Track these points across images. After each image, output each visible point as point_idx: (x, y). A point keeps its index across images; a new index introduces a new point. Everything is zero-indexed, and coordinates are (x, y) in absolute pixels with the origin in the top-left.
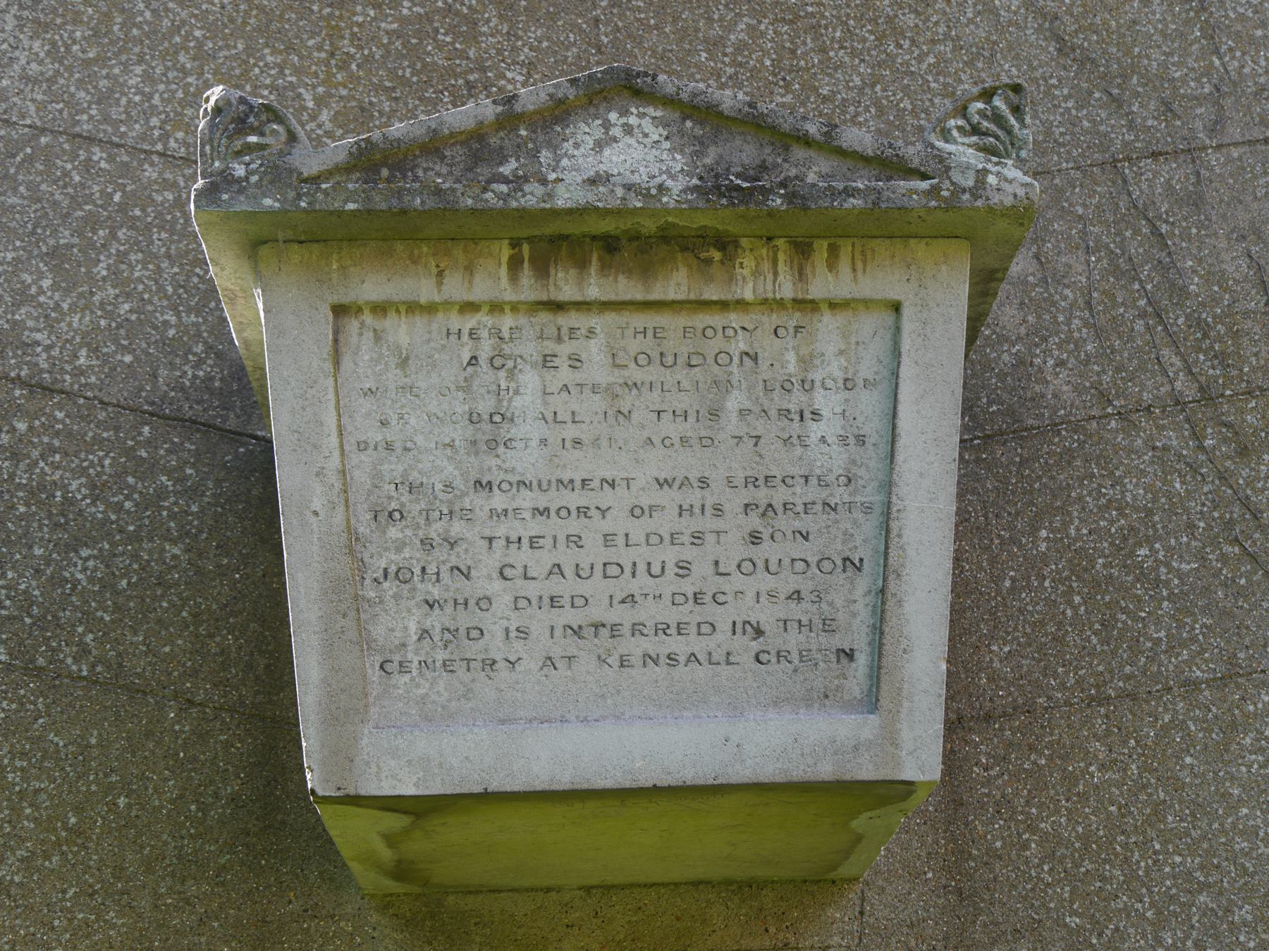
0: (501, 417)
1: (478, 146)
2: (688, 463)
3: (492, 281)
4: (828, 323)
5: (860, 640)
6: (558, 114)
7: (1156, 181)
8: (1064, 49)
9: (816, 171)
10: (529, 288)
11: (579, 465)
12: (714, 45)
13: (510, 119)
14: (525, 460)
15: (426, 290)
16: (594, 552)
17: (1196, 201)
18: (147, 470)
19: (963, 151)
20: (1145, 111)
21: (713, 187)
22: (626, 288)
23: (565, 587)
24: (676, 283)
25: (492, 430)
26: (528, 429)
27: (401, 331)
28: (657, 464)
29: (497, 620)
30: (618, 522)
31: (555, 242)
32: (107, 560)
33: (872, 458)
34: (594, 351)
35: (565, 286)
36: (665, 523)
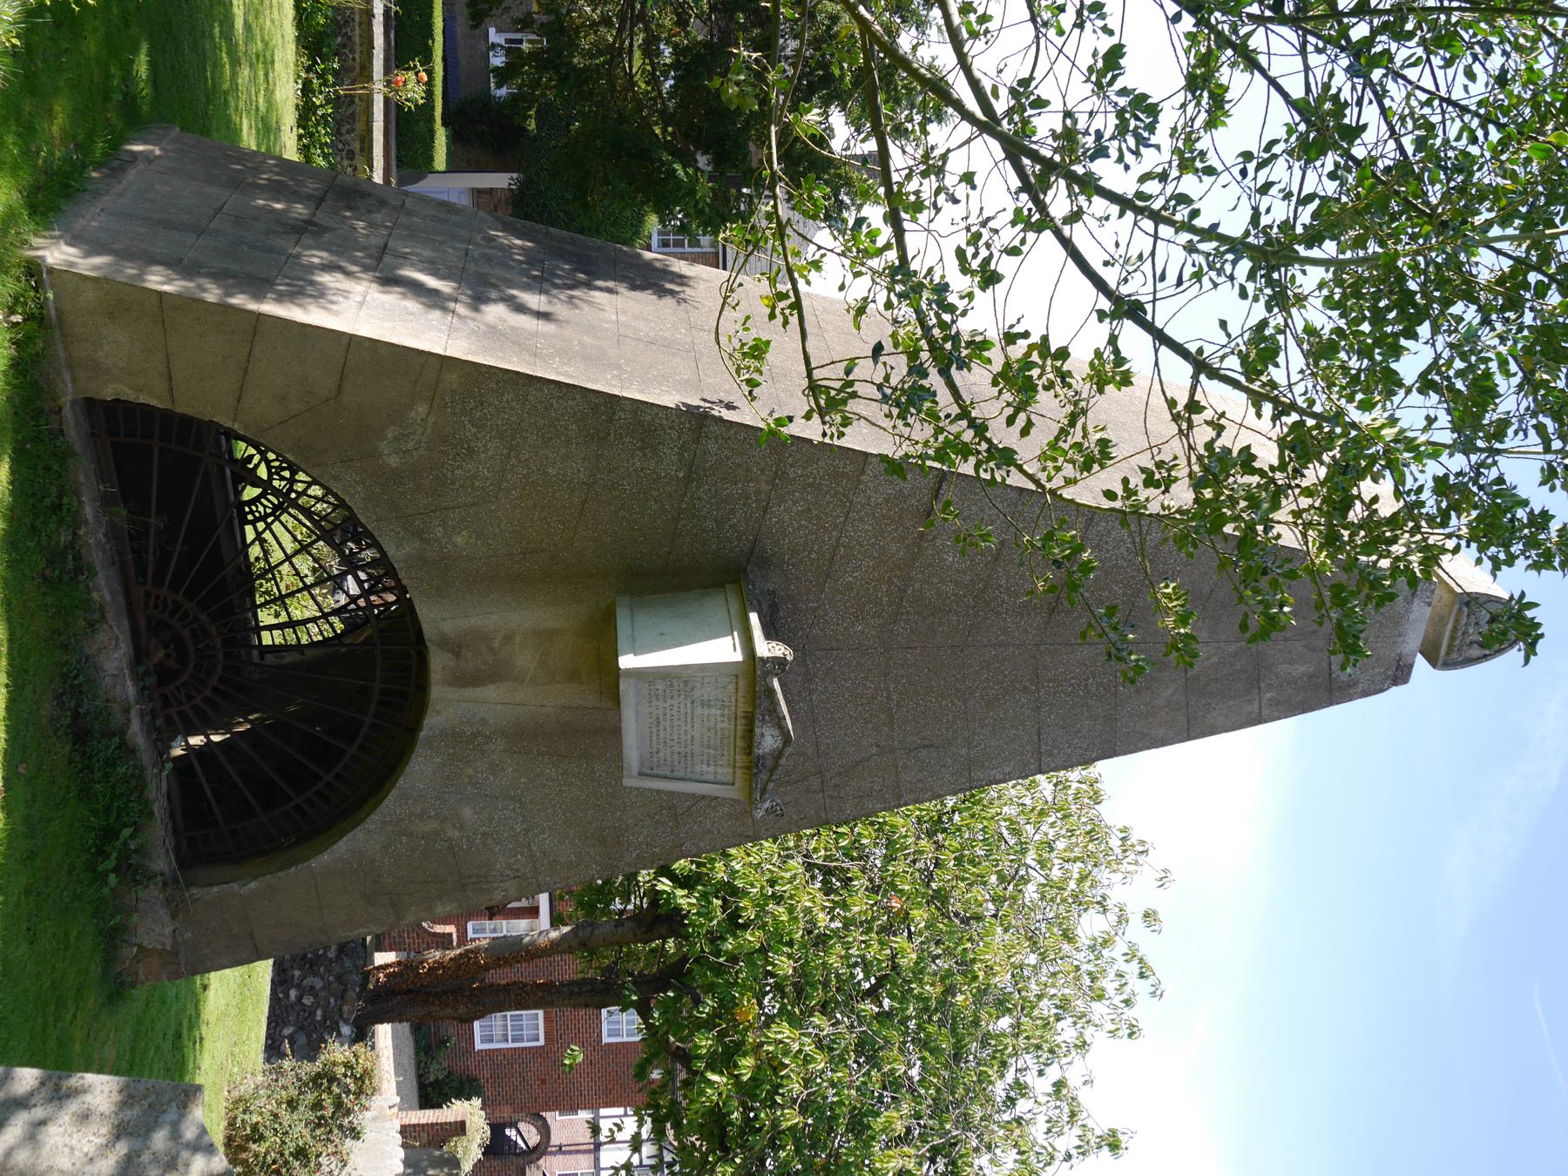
0: (709, 706)
2: (697, 741)
3: (742, 708)
4: (730, 770)
5: (656, 771)
7: (816, 783)
8: (858, 763)
9: (764, 776)
10: (740, 714)
11: (697, 721)
12: (866, 678)
14: (699, 710)
16: (676, 723)
17: (808, 791)
18: (739, 538)
19: (767, 805)
20: (837, 780)
22: (740, 733)
24: (740, 743)
25: (706, 704)
26: (706, 711)
27: (731, 687)
28: (697, 736)
29: (661, 704)
30: (683, 728)
31: (749, 735)
32: (712, 530)
33: (696, 777)
35: (741, 722)
36: (683, 737)
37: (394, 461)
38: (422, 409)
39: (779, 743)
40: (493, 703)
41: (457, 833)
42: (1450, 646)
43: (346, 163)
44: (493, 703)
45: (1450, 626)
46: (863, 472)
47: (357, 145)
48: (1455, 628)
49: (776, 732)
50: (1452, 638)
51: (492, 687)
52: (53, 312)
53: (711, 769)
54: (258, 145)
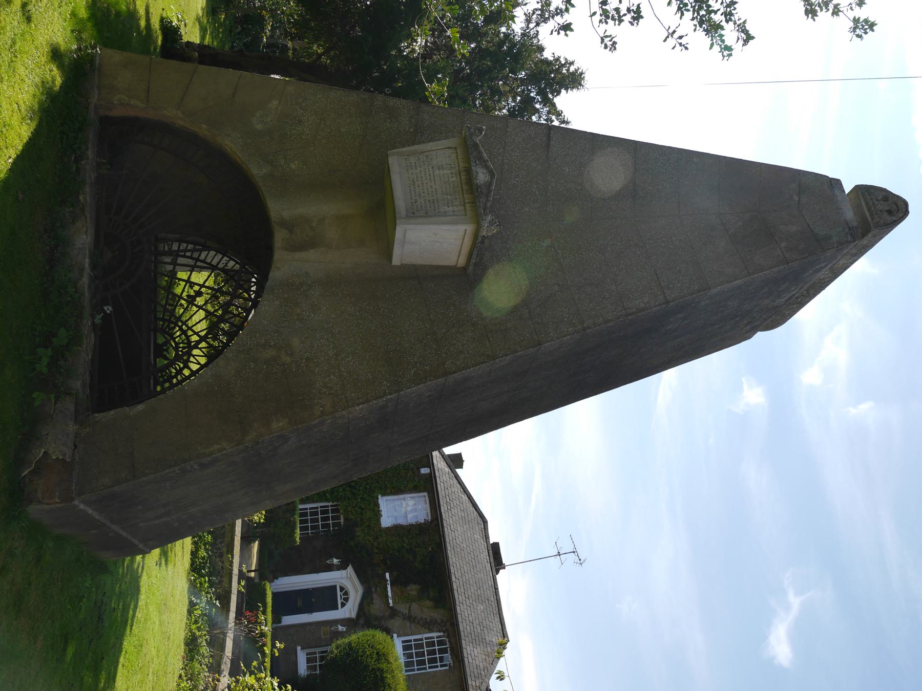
1: (480, 158)
6: (487, 167)
13: (485, 161)
14: (437, 172)
15: (460, 157)
21: (478, 187)
23: (420, 179)
24: (465, 187)
25: (441, 168)
27: (454, 156)
31: (468, 171)
34: (454, 179)
37: (259, 127)
38: (275, 103)
39: (488, 178)
40: (312, 262)
41: (288, 359)
42: (871, 214)
43: (218, 560)
44: (312, 262)
45: (863, 203)
46: (507, 127)
47: (225, 550)
48: (867, 204)
49: (485, 171)
50: (869, 209)
51: (312, 251)
52: (97, 62)
53: (451, 209)
54: (203, 38)
